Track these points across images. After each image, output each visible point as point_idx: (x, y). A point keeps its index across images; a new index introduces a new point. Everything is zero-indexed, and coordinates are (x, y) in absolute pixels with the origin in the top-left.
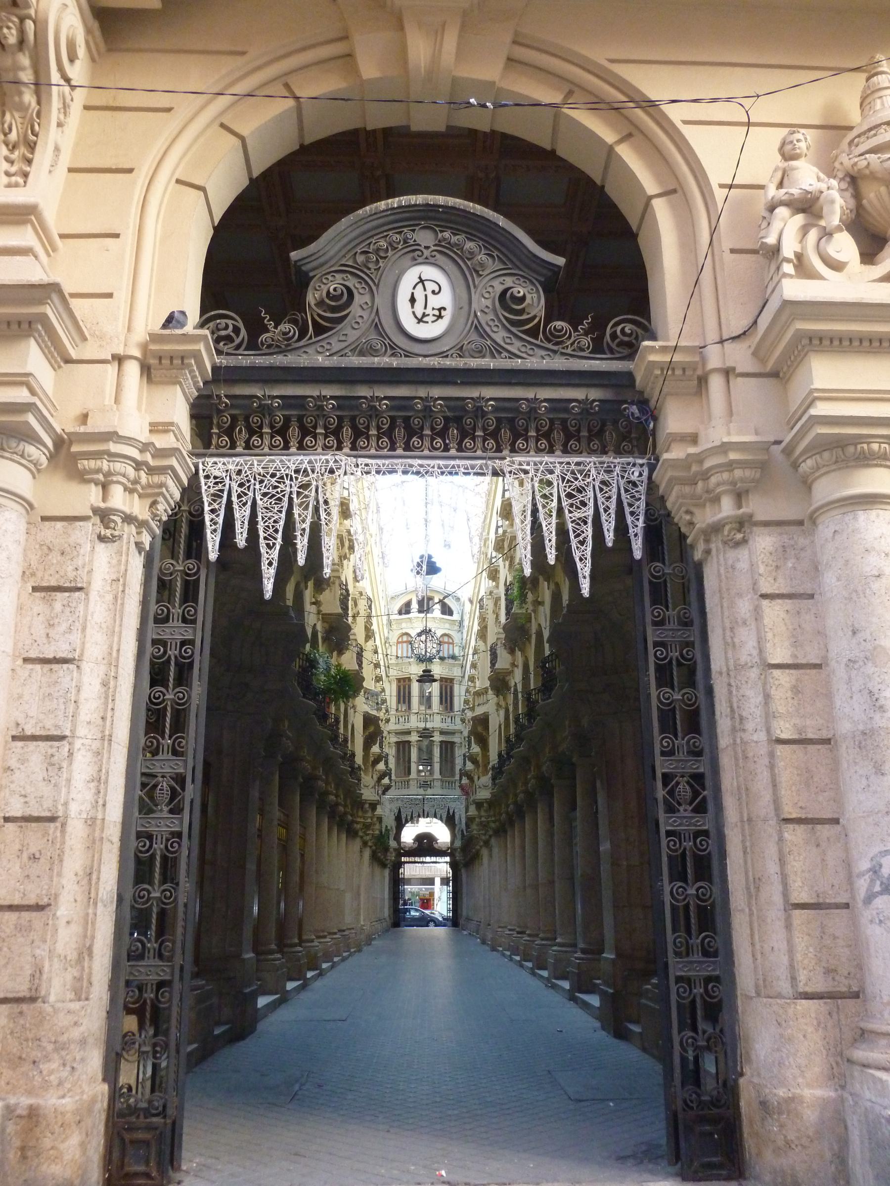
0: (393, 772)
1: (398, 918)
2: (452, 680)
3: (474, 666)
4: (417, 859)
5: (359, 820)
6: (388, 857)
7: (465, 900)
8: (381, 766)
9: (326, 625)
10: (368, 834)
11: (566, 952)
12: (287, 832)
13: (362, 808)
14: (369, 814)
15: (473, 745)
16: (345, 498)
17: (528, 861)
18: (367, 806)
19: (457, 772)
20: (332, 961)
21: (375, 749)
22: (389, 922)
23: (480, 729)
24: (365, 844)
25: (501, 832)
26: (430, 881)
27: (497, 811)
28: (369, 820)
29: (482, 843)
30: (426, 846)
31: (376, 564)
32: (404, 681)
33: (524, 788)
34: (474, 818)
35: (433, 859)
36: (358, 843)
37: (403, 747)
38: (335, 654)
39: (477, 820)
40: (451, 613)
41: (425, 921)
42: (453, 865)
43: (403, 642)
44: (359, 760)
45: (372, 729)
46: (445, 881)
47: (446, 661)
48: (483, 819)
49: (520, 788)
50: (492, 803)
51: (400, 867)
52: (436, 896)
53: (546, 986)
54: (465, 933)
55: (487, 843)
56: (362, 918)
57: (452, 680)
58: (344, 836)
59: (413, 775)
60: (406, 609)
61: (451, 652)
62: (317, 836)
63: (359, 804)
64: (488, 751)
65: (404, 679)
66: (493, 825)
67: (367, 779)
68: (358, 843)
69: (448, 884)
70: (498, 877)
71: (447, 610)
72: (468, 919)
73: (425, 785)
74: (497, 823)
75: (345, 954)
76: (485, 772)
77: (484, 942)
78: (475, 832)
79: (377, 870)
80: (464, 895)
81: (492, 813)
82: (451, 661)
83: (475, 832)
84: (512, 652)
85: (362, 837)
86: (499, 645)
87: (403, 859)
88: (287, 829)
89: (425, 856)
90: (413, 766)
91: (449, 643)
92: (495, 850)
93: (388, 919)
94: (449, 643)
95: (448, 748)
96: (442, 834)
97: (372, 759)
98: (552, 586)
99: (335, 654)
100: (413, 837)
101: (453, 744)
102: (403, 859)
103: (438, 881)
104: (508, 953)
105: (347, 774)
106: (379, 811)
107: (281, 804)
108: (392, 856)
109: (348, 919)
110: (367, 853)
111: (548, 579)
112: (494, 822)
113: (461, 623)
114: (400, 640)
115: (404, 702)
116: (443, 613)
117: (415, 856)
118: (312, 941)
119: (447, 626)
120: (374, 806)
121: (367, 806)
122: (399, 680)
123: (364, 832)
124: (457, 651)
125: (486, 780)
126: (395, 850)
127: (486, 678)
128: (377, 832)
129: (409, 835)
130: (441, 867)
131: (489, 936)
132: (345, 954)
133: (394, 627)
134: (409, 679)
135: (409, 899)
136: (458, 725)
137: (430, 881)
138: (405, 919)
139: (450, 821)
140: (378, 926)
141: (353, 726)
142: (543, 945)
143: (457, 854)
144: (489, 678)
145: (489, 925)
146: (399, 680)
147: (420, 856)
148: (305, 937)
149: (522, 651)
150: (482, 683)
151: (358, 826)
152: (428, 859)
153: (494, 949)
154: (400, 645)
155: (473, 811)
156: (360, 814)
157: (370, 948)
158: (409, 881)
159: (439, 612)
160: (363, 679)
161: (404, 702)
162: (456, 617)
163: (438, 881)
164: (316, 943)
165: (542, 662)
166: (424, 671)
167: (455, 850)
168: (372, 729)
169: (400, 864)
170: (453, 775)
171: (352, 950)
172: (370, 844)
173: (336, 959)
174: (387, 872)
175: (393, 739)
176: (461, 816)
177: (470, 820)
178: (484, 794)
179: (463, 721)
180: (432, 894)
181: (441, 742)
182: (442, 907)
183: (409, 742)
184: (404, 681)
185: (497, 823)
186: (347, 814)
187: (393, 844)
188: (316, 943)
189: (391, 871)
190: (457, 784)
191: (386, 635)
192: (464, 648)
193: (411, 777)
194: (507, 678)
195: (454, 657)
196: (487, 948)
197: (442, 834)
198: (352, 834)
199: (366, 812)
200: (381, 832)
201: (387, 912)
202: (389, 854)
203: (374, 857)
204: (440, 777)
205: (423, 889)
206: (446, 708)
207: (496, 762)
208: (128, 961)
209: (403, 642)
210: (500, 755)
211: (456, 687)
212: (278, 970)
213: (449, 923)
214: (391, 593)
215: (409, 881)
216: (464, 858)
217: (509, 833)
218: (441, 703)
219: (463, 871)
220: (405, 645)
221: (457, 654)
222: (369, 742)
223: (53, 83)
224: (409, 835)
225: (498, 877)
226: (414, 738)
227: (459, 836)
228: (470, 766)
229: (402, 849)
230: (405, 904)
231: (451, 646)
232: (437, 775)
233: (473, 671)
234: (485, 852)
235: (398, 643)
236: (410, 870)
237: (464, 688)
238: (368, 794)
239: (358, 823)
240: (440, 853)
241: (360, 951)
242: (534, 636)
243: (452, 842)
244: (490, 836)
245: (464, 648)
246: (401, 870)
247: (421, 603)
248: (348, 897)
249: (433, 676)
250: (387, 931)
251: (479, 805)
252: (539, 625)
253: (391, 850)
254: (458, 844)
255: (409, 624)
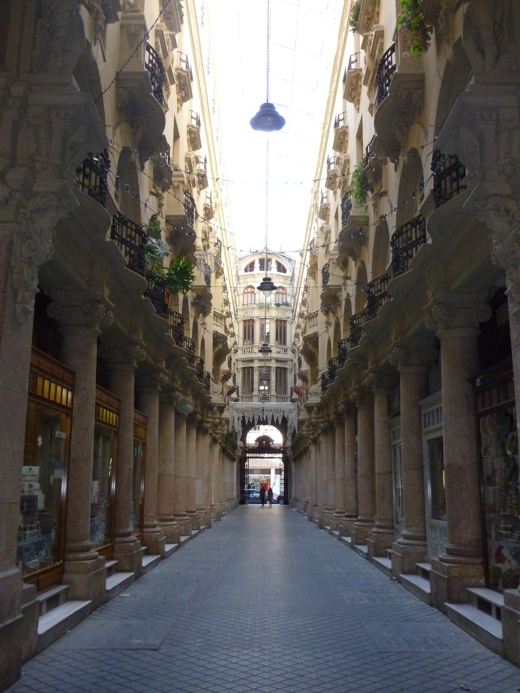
0: (240, 389)
1: (244, 498)
2: (285, 322)
3: (304, 303)
4: (258, 455)
5: (209, 420)
6: (234, 452)
7: (293, 485)
8: (230, 383)
9: (170, 227)
10: (218, 434)
11: (415, 545)
12: (119, 420)
13: (212, 410)
14: (218, 415)
15: (294, 393)
16: (208, 205)
17: (361, 453)
18: (216, 408)
19: (289, 390)
20: (178, 541)
21: (224, 366)
22: (237, 500)
23: (310, 347)
24: (215, 441)
25: (329, 430)
26: (268, 471)
27: (325, 413)
28: (218, 420)
29: (310, 442)
30: (264, 446)
31: (231, 255)
32: (249, 322)
33: (357, 386)
34: (304, 421)
35: (270, 455)
36: (208, 440)
37: (248, 372)
38: (201, 315)
39: (307, 423)
40: (284, 271)
41: (262, 500)
42: (285, 460)
43: (248, 293)
44: (209, 367)
45: (220, 346)
46: (278, 471)
47: (281, 307)
48: (313, 420)
49: (341, 399)
50: (321, 407)
51: (245, 461)
52: (272, 482)
53: (391, 579)
54: (294, 510)
55: (315, 441)
56: (213, 500)
57: (285, 322)
58: (194, 433)
59: (255, 393)
60: (251, 267)
61: (284, 301)
62: (160, 428)
63: (207, 406)
64: (317, 365)
65: (249, 321)
66: (322, 425)
67: (215, 387)
68: (208, 440)
69: (280, 474)
70: (325, 468)
71: (281, 268)
72: (296, 500)
73: (265, 398)
74: (326, 424)
75: (194, 532)
76: (315, 382)
77: (311, 519)
78: (305, 432)
79: (228, 463)
80: (293, 481)
81: (320, 415)
82: (284, 307)
83: (305, 432)
84: (327, 313)
85: (211, 434)
86: (355, 192)
87: (248, 455)
88: (117, 414)
89: (264, 453)
90: (256, 386)
91: (283, 294)
92: (323, 447)
93: (236, 498)
94: (283, 294)
95: (281, 372)
96: (277, 437)
97: (222, 375)
98: (359, 264)
99: (201, 315)
100: (256, 438)
101: (285, 369)
102: (248, 455)
103: (273, 471)
104: (337, 533)
105: (197, 383)
106: (226, 414)
107: (138, 405)
108: (239, 453)
109: (199, 501)
110: (217, 449)
111: (355, 259)
112: (322, 422)
113: (292, 278)
114: (246, 291)
115: (249, 339)
116: (279, 270)
117: (256, 453)
118: (155, 526)
119: (282, 280)
120: (221, 409)
121: (216, 408)
122: (245, 321)
123: (214, 430)
124: (289, 299)
125: (316, 388)
126: (241, 448)
127: (319, 297)
128: (226, 432)
129: (252, 438)
130: (276, 461)
131: (317, 515)
132: (194, 532)
133: (241, 281)
134: (253, 321)
135: (252, 484)
136: (289, 355)
137: (268, 471)
138: (249, 498)
139: (282, 425)
140: (227, 504)
141: (203, 341)
142: (380, 533)
143: (288, 452)
144: (322, 297)
145: (315, 506)
146: (245, 321)
147: (260, 453)
148: (146, 523)
149: (334, 313)
150: (316, 305)
151: (208, 425)
152: (266, 455)
153: (321, 527)
154: (245, 295)
155: (304, 415)
156: (210, 415)
157: (220, 524)
158: (252, 471)
159: (276, 270)
160: (210, 297)
161: (249, 339)
162: (289, 273)
163: (273, 471)
164: (158, 529)
165: (350, 320)
166: (264, 279)
167: (287, 448)
168: (220, 346)
169: (245, 459)
170: (285, 392)
171: (202, 527)
172: (219, 441)
173: (183, 539)
174: (235, 464)
175: (241, 365)
176: (293, 420)
177: (301, 423)
178: (314, 400)
179: (293, 351)
180: (269, 480)
181: (277, 368)
182: (277, 489)
183: (252, 368)
184: (249, 322)
185: (326, 424)
186: (201, 419)
187: (240, 443)
188: (158, 529)
189: (238, 463)
190: (289, 399)
191: (235, 286)
192: (294, 297)
193: (254, 394)
194: (338, 294)
195: (287, 304)
196: (315, 525)
197: (277, 437)
198: (202, 431)
199: (215, 413)
200: (228, 431)
201: (235, 494)
202: (237, 451)
203: (223, 451)
204: (275, 394)
205: (262, 477)
206: (281, 343)
207: (326, 370)
208: (440, 439)
209: (248, 293)
210: (330, 362)
211: (288, 326)
212: (89, 572)
213: (282, 501)
214: (240, 255)
215: (252, 471)
216: (294, 455)
217: (337, 430)
218: (277, 340)
219: (293, 464)
220: (249, 295)
221: (289, 302)
222: (219, 358)
223: (164, 266)
224: (252, 438)
225: (325, 468)
226: (256, 364)
227: (290, 438)
228: (299, 383)
229: (247, 447)
230: (249, 487)
231: (284, 296)
232: (273, 393)
233: (304, 309)
234: (312, 448)
235: (244, 293)
236: (253, 463)
237: (294, 326)
238: (216, 399)
239: (208, 422)
240: (275, 451)
241: (209, 527)
242: (344, 303)
243: (285, 443)
244: (319, 434)
245: (294, 297)
246: (246, 463)
247: (262, 261)
248: (199, 484)
249: (273, 284)
250: (235, 507)
251: (309, 409)
252: (348, 294)
253: (239, 448)
254: (289, 444)
255: (253, 279)
